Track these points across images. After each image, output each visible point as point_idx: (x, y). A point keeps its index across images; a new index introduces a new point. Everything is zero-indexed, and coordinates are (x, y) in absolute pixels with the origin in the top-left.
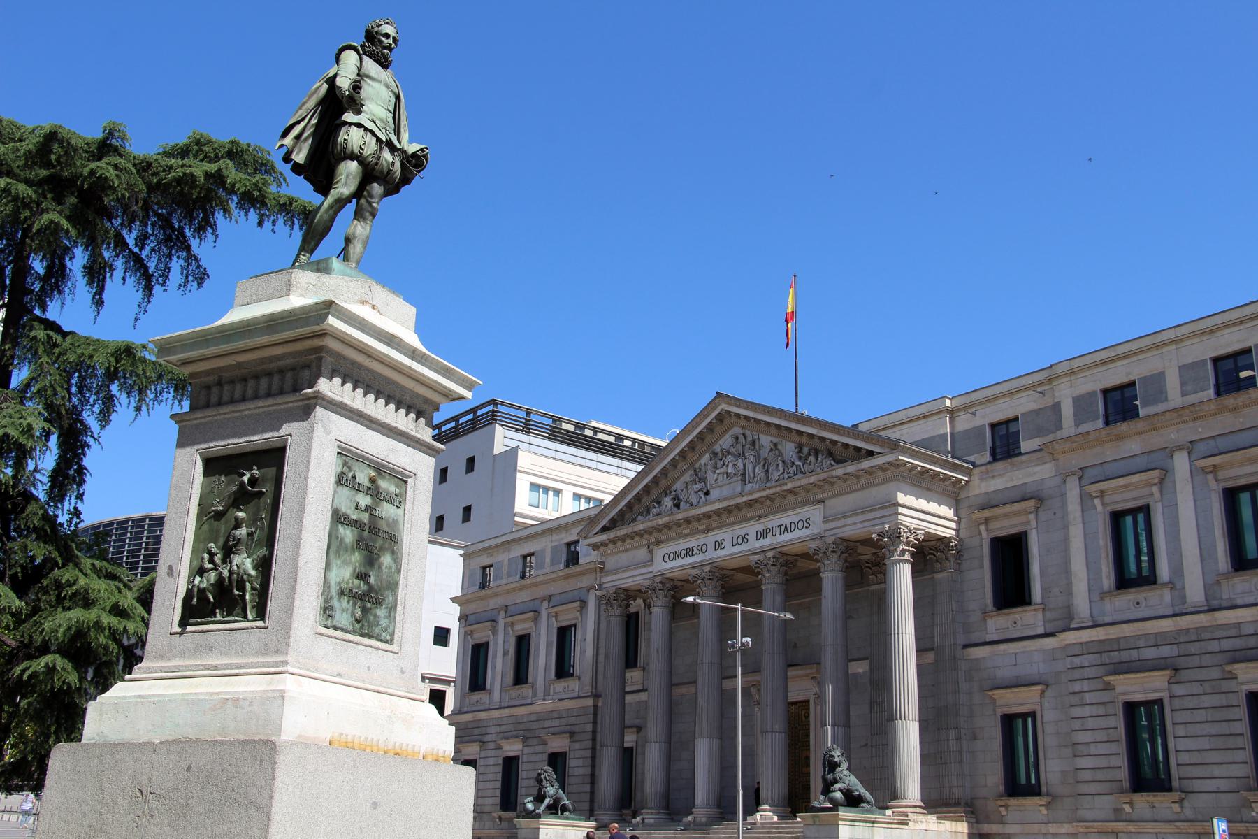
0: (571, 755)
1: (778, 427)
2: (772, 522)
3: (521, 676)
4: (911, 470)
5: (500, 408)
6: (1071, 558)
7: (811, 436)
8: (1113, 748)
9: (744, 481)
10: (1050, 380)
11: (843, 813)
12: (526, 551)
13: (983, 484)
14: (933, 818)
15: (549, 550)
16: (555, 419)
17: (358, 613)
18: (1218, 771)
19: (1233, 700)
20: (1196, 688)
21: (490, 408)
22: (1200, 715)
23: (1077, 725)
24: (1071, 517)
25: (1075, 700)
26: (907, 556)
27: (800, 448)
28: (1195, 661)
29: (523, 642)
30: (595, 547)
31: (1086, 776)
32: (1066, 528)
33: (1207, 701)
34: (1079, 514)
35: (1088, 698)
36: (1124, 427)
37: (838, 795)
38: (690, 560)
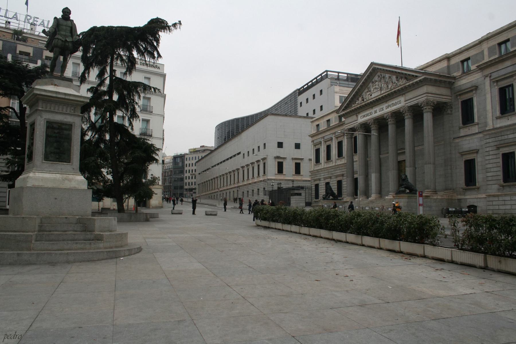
0: (343, 181)
2: (390, 103)
3: (328, 157)
9: (381, 90)
12: (327, 119)
17: (57, 157)
21: (325, 73)
23: (487, 162)
25: (487, 154)
27: (397, 78)
29: (329, 148)
31: (490, 178)
32: (485, 95)
34: (489, 89)
35: (491, 153)
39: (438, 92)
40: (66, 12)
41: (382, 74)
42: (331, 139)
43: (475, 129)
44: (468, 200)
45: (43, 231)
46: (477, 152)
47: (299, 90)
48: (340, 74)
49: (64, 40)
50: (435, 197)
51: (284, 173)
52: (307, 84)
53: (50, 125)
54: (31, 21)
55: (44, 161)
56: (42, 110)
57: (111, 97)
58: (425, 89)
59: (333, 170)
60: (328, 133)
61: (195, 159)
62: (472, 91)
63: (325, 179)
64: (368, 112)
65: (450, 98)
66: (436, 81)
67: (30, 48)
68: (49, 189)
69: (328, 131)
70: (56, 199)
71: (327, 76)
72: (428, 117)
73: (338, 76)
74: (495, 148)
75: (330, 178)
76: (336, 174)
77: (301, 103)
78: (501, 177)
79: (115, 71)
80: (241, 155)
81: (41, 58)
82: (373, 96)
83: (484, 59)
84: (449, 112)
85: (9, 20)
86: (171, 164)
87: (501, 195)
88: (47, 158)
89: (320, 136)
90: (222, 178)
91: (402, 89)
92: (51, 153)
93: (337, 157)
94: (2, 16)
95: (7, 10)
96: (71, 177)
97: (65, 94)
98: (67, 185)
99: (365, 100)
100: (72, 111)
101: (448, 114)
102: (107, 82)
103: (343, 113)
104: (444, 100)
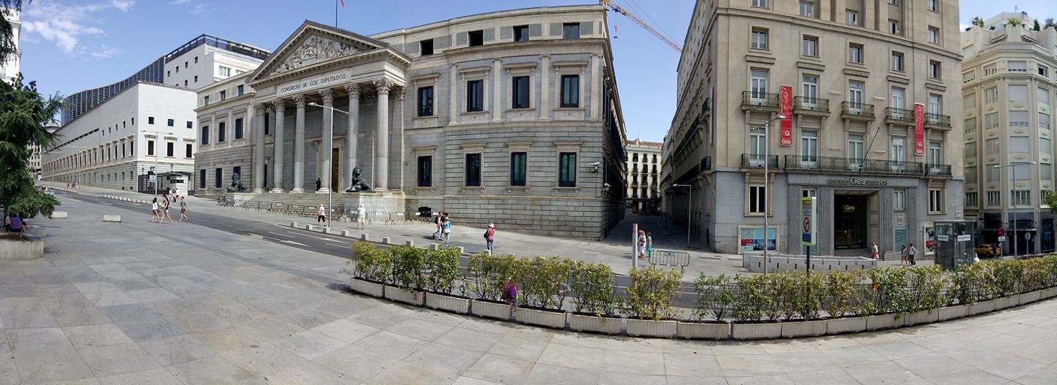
1: (333, 35)
2: (329, 75)
4: (390, 56)
5: (206, 37)
6: (450, 97)
7: (348, 39)
8: (461, 170)
10: (448, 26)
11: (362, 193)
13: (417, 65)
14: (391, 193)
15: (231, 89)
16: (229, 42)
18: (497, 179)
19: (506, 155)
20: (494, 150)
21: (202, 37)
22: (494, 160)
24: (452, 82)
26: (387, 92)
28: (494, 140)
30: (252, 86)
31: (450, 180)
32: (449, 86)
33: (497, 155)
35: (453, 152)
36: (477, 48)
37: (359, 186)
38: (293, 91)
41: (318, 37)
42: (227, 115)
44: (420, 202)
60: (206, 112)
64: (292, 84)
69: (222, 104)
77: (169, 72)
78: (464, 179)
82: (304, 64)
87: (461, 198)
89: (210, 111)
91: (350, 60)
93: (234, 138)
99: (290, 69)
103: (256, 82)
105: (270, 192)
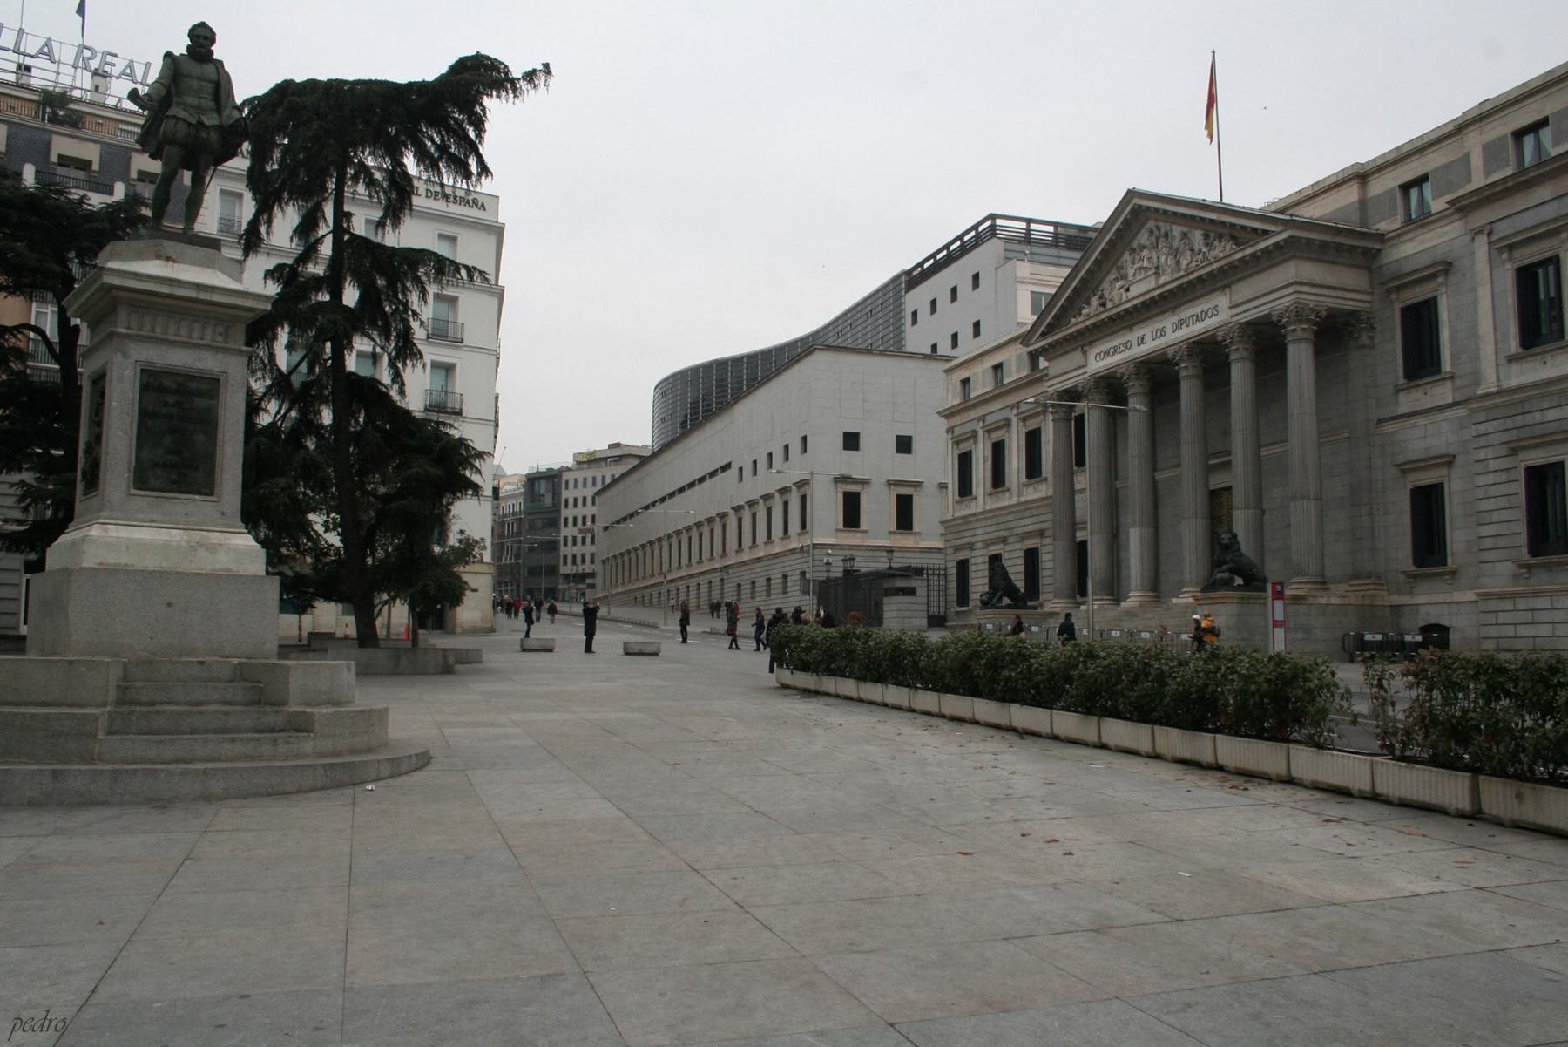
0: (1043, 550)
2: (1186, 313)
3: (998, 478)
9: (1157, 274)
12: (995, 362)
17: (174, 477)
21: (989, 223)
23: (1480, 493)
25: (1479, 468)
27: (1206, 236)
29: (998, 450)
31: (1489, 543)
32: (1474, 289)
34: (1487, 272)
35: (1492, 465)
39: (1330, 281)
40: (202, 37)
41: (1161, 225)
42: (1007, 423)
43: (1442, 393)
44: (1423, 610)
45: (131, 703)
46: (1450, 464)
47: (908, 273)
48: (1033, 226)
49: (194, 122)
50: (1323, 601)
51: (864, 525)
52: (933, 256)
53: (153, 382)
54: (94, 64)
55: (133, 491)
56: (126, 336)
57: (337, 294)
58: (1290, 271)
59: (1011, 517)
60: (997, 405)
61: (594, 484)
62: (1433, 276)
63: (988, 543)
64: (1118, 341)
65: (1367, 298)
66: (1324, 245)
67: (92, 145)
68: (150, 574)
69: (996, 397)
70: (169, 605)
71: (992, 230)
72: (1300, 357)
73: (1028, 230)
74: (1503, 450)
75: (1004, 541)
76: (1020, 530)
77: (915, 314)
78: (1522, 540)
79: (349, 215)
80: (734, 471)
81: (125, 177)
82: (1134, 291)
83: (1470, 181)
84: (1365, 340)
85: (28, 61)
86: (521, 500)
87: (1522, 595)
88: (142, 479)
89: (973, 414)
90: (675, 541)
91: (1221, 269)
92: (156, 465)
93: (1024, 479)
94: (7, 50)
95: (21, 31)
96: (215, 537)
97: (199, 287)
98: (205, 563)
99: (1109, 305)
100: (220, 339)
101: (1362, 346)
102: (326, 249)
103: (1043, 343)
104: (1349, 305)
105: (1083, 607)
